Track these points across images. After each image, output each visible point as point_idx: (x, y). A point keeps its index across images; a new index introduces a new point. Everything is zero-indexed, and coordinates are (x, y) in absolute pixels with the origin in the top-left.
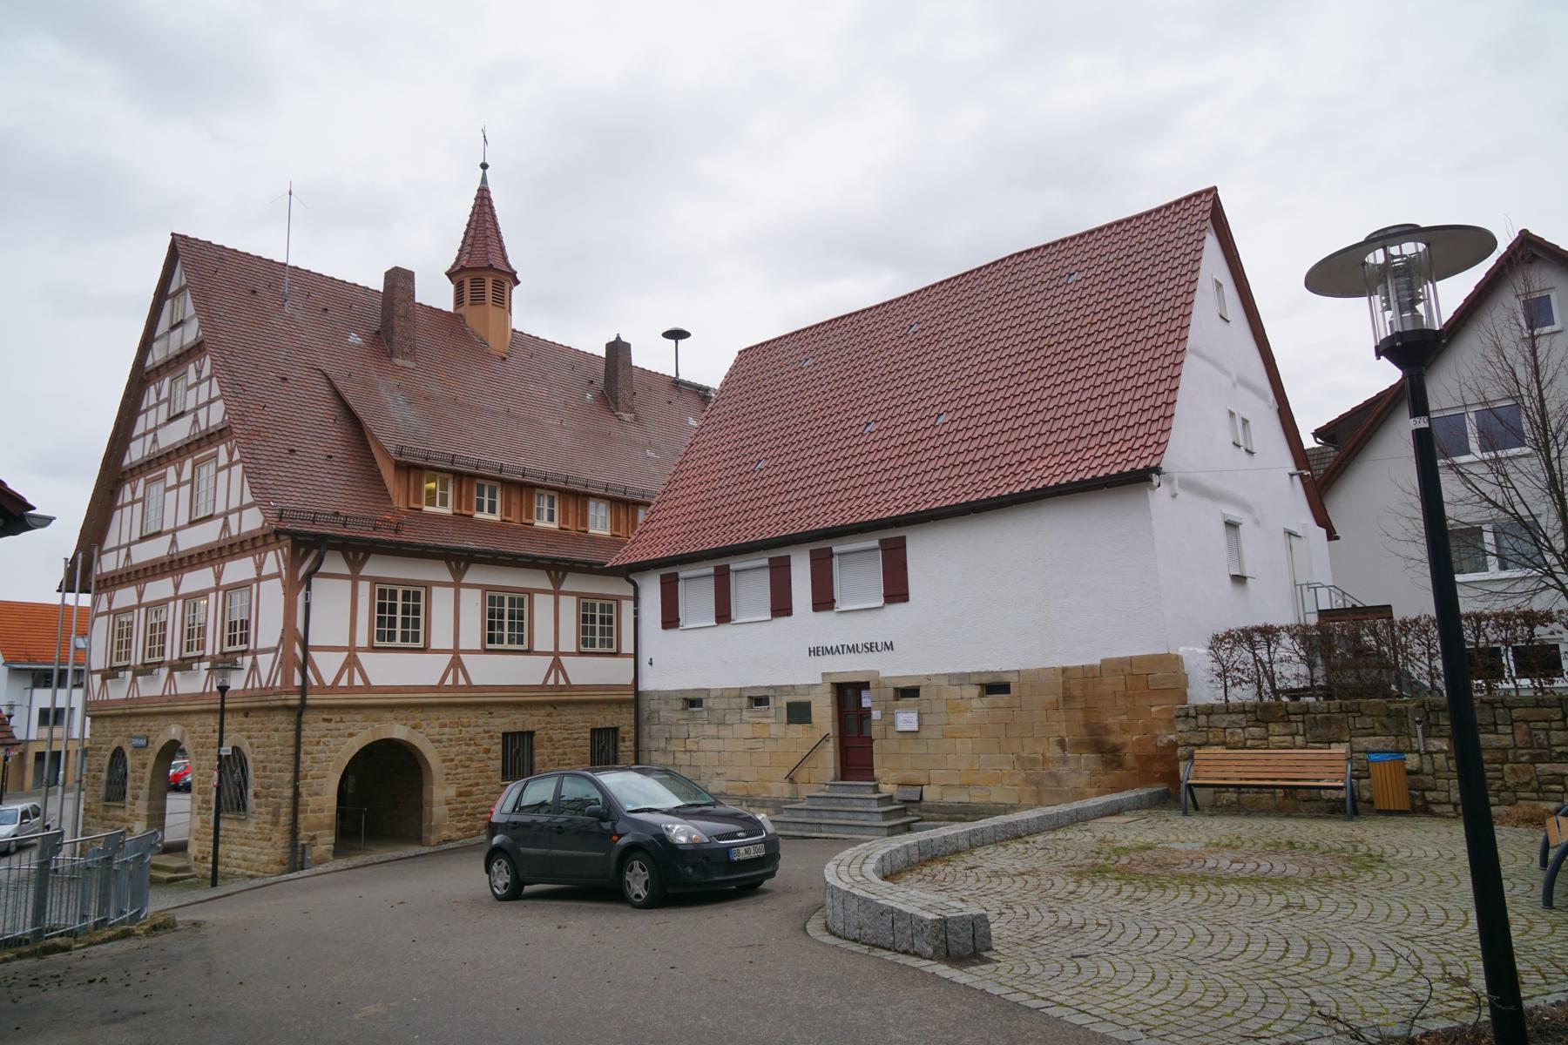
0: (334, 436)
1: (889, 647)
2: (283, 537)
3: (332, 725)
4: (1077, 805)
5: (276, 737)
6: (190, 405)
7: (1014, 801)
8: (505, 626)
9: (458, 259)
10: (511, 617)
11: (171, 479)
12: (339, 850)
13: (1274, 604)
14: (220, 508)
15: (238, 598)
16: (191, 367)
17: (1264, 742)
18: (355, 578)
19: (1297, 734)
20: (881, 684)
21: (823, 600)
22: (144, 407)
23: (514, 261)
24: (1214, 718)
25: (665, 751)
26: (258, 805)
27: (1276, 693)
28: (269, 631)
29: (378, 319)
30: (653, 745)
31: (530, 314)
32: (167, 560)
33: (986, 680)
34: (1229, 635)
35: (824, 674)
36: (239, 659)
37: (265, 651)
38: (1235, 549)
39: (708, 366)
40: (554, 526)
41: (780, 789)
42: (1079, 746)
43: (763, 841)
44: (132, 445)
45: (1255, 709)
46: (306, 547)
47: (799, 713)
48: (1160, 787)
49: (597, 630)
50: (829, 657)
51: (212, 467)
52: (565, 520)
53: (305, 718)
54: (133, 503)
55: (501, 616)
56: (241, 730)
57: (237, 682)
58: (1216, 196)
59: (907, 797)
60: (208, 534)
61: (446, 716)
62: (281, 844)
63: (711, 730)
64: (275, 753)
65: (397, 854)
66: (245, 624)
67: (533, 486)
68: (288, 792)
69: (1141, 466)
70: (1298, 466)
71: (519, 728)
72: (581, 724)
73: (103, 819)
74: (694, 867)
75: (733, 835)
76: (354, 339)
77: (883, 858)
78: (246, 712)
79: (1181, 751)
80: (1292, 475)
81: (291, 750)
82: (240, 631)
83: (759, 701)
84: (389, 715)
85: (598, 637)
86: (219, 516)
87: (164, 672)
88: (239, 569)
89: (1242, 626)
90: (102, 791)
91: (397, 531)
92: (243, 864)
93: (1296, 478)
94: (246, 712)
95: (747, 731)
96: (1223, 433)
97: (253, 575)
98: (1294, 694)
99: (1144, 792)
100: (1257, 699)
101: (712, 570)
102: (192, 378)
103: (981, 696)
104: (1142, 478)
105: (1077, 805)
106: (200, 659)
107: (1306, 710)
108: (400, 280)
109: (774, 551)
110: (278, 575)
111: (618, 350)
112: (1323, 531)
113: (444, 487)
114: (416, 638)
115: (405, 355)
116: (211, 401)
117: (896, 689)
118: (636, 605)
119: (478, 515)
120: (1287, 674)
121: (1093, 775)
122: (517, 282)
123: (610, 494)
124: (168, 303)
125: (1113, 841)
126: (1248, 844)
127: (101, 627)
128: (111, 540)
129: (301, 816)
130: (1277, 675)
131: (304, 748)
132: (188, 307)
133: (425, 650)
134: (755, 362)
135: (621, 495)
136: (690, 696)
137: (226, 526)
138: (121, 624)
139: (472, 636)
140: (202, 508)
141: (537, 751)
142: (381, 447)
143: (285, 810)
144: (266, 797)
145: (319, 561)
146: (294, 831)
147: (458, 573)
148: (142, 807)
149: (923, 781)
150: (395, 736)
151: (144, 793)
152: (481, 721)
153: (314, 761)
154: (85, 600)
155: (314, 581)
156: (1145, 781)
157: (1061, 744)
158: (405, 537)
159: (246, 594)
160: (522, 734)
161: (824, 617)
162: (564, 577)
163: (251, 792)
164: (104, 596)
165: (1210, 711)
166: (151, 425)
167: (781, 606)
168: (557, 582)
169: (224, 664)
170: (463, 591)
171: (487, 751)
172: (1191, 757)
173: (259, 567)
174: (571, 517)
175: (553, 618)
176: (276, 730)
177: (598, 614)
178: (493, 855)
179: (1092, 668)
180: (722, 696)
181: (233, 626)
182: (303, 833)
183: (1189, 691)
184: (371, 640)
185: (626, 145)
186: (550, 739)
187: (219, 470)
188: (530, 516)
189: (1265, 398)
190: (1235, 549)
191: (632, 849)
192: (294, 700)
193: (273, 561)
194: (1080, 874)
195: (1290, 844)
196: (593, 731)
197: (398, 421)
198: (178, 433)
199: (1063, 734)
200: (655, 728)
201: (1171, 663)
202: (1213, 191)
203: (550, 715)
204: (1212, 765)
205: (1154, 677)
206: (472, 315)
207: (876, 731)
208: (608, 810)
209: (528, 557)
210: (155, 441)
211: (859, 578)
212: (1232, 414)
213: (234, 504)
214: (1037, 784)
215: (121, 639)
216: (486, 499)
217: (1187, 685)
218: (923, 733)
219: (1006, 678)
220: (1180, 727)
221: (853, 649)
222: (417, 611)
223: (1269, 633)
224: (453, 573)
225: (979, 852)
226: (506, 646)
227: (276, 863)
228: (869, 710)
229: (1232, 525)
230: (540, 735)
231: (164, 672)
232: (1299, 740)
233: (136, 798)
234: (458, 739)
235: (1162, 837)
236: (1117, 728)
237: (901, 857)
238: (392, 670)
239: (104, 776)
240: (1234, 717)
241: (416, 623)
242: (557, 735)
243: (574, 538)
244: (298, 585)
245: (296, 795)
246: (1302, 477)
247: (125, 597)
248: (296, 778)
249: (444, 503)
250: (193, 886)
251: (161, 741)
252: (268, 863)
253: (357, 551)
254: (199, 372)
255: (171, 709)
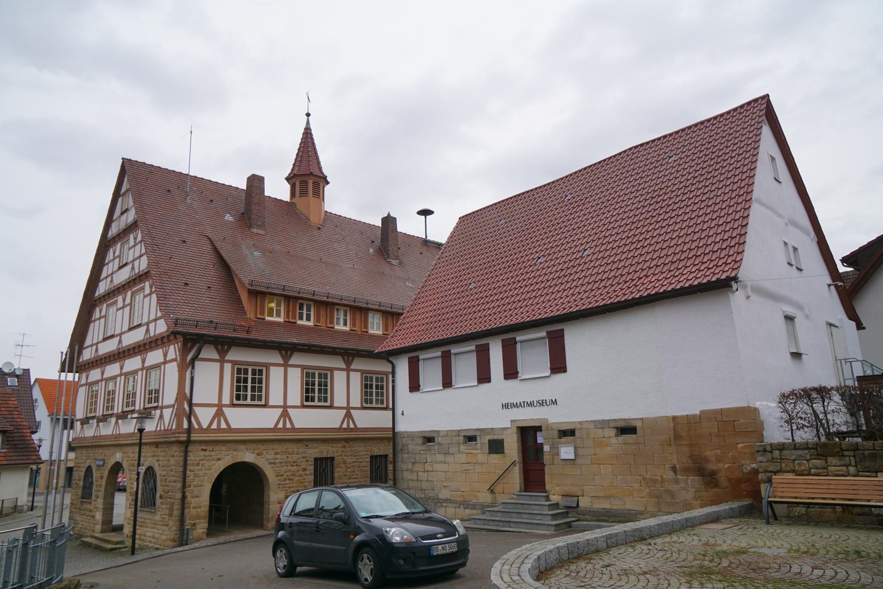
0: (212, 274)
1: (554, 402)
2: (178, 336)
3: (207, 453)
4: (686, 515)
5: (173, 461)
6: (131, 259)
7: (642, 508)
8: (316, 391)
9: (292, 170)
10: (320, 385)
11: (120, 304)
12: (210, 533)
13: (820, 372)
14: (145, 320)
15: (154, 374)
16: (132, 236)
17: (824, 471)
18: (222, 361)
19: (850, 465)
20: (549, 428)
21: (511, 373)
22: (107, 261)
23: (325, 171)
24: (785, 452)
25: (412, 471)
26: (162, 503)
27: (829, 435)
28: (169, 396)
29: (243, 206)
30: (404, 467)
31: (339, 200)
32: (116, 352)
33: (621, 424)
34: (793, 393)
35: (512, 421)
36: (153, 412)
37: (168, 407)
38: (793, 335)
39: (440, 230)
40: (347, 328)
41: (485, 497)
42: (686, 471)
43: (457, 541)
44: (100, 284)
45: (816, 446)
46: (192, 341)
47: (496, 446)
48: (747, 502)
49: (376, 393)
50: (515, 410)
51: (142, 295)
52: (354, 324)
53: (190, 449)
54: (100, 318)
55: (313, 385)
56: (154, 456)
57: (150, 426)
58: (769, 100)
59: (568, 504)
60: (137, 336)
61: (278, 448)
62: (174, 528)
63: (440, 457)
64: (172, 470)
65: (249, 535)
66: (157, 391)
67: (333, 304)
68: (179, 496)
69: (723, 277)
70: (833, 279)
71: (325, 455)
72: (364, 453)
73: (80, 509)
74: (405, 560)
75: (433, 536)
76: (228, 218)
77: (539, 558)
78: (157, 445)
79: (761, 476)
80: (829, 285)
81: (181, 469)
82: (154, 395)
83: (471, 439)
84: (242, 447)
85: (374, 398)
86: (144, 325)
87: (113, 420)
88: (154, 357)
89: (803, 387)
90: (80, 492)
91: (248, 332)
92: (153, 540)
93: (832, 287)
94: (157, 445)
95: (463, 458)
96: (781, 257)
97: (162, 360)
98: (842, 435)
99: (735, 505)
100: (816, 439)
101: (440, 354)
102: (132, 243)
103: (617, 435)
104: (723, 286)
105: (686, 515)
106: (133, 412)
107: (856, 448)
108: (256, 182)
109: (479, 339)
110: (175, 360)
111: (389, 222)
112: (853, 324)
113: (278, 305)
114: (260, 399)
115: (259, 227)
116: (141, 256)
117: (559, 431)
118: (393, 377)
119: (299, 322)
120: (838, 421)
121: (697, 491)
122: (328, 183)
123: (382, 308)
124: (120, 199)
125: (714, 545)
126: (822, 552)
127: (82, 393)
128: (88, 342)
129: (186, 511)
130: (831, 422)
131: (189, 467)
132: (130, 201)
133: (265, 406)
134: (468, 224)
135: (389, 309)
136: (427, 435)
137: (148, 330)
138: (93, 391)
139: (295, 396)
140: (136, 320)
141: (336, 470)
142: (240, 281)
143: (177, 507)
144: (167, 498)
145: (199, 352)
146: (182, 521)
147: (286, 358)
148: (100, 503)
149: (579, 493)
150: (247, 460)
151: (101, 494)
152: (301, 451)
153: (195, 476)
154: (70, 377)
155: (197, 363)
156: (736, 497)
157: (674, 469)
158: (252, 336)
159: (158, 372)
160: (326, 458)
161: (511, 383)
162: (353, 360)
163: (158, 495)
164: (84, 375)
165: (782, 447)
166: (110, 272)
167: (484, 377)
168: (348, 363)
169: (146, 414)
170: (289, 369)
171: (305, 470)
172: (769, 481)
173: (165, 355)
174: (358, 323)
175: (346, 386)
176: (173, 456)
177: (374, 383)
178: (278, 544)
179: (694, 416)
180: (447, 435)
181: (150, 392)
182: (187, 522)
183: (765, 433)
184: (232, 400)
185: (414, 121)
186: (345, 462)
187: (145, 297)
188: (332, 323)
189: (808, 234)
190: (793, 335)
191: (363, 545)
192: (183, 437)
193: (173, 351)
194: (690, 575)
195: (858, 552)
196: (372, 457)
197: (253, 264)
198: (124, 275)
199: (675, 462)
200: (405, 456)
201: (751, 413)
202: (768, 95)
203: (344, 447)
204: (786, 487)
205: (739, 423)
206: (300, 202)
207: (546, 459)
208: (346, 519)
209: (330, 347)
210: (112, 281)
211: (534, 357)
212: (786, 244)
213: (152, 317)
214: (657, 497)
215: (92, 398)
216: (305, 312)
217: (763, 429)
218: (579, 461)
219: (634, 424)
220: (760, 458)
221: (531, 404)
222: (260, 382)
223: (823, 392)
224: (283, 358)
225: (614, 552)
226: (316, 403)
227: (171, 541)
228: (542, 444)
229: (789, 319)
230: (338, 459)
231: (113, 420)
232: (852, 469)
233: (97, 497)
234: (286, 462)
235: (753, 543)
236: (713, 459)
237: (554, 556)
238: (244, 418)
239: (81, 483)
240: (800, 452)
241: (260, 389)
242: (349, 460)
243: (359, 336)
244: (187, 365)
245: (184, 497)
246: (836, 287)
247: (95, 374)
248: (184, 486)
249: (278, 315)
250: (122, 554)
251: (111, 462)
252: (166, 540)
253: (223, 344)
254: (135, 239)
255: (116, 443)
